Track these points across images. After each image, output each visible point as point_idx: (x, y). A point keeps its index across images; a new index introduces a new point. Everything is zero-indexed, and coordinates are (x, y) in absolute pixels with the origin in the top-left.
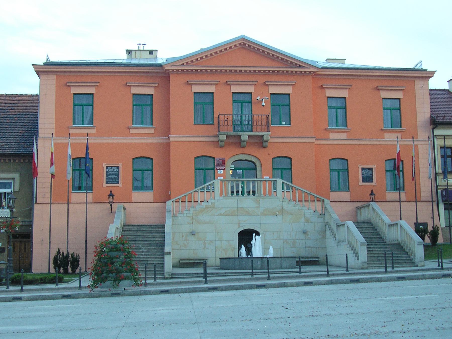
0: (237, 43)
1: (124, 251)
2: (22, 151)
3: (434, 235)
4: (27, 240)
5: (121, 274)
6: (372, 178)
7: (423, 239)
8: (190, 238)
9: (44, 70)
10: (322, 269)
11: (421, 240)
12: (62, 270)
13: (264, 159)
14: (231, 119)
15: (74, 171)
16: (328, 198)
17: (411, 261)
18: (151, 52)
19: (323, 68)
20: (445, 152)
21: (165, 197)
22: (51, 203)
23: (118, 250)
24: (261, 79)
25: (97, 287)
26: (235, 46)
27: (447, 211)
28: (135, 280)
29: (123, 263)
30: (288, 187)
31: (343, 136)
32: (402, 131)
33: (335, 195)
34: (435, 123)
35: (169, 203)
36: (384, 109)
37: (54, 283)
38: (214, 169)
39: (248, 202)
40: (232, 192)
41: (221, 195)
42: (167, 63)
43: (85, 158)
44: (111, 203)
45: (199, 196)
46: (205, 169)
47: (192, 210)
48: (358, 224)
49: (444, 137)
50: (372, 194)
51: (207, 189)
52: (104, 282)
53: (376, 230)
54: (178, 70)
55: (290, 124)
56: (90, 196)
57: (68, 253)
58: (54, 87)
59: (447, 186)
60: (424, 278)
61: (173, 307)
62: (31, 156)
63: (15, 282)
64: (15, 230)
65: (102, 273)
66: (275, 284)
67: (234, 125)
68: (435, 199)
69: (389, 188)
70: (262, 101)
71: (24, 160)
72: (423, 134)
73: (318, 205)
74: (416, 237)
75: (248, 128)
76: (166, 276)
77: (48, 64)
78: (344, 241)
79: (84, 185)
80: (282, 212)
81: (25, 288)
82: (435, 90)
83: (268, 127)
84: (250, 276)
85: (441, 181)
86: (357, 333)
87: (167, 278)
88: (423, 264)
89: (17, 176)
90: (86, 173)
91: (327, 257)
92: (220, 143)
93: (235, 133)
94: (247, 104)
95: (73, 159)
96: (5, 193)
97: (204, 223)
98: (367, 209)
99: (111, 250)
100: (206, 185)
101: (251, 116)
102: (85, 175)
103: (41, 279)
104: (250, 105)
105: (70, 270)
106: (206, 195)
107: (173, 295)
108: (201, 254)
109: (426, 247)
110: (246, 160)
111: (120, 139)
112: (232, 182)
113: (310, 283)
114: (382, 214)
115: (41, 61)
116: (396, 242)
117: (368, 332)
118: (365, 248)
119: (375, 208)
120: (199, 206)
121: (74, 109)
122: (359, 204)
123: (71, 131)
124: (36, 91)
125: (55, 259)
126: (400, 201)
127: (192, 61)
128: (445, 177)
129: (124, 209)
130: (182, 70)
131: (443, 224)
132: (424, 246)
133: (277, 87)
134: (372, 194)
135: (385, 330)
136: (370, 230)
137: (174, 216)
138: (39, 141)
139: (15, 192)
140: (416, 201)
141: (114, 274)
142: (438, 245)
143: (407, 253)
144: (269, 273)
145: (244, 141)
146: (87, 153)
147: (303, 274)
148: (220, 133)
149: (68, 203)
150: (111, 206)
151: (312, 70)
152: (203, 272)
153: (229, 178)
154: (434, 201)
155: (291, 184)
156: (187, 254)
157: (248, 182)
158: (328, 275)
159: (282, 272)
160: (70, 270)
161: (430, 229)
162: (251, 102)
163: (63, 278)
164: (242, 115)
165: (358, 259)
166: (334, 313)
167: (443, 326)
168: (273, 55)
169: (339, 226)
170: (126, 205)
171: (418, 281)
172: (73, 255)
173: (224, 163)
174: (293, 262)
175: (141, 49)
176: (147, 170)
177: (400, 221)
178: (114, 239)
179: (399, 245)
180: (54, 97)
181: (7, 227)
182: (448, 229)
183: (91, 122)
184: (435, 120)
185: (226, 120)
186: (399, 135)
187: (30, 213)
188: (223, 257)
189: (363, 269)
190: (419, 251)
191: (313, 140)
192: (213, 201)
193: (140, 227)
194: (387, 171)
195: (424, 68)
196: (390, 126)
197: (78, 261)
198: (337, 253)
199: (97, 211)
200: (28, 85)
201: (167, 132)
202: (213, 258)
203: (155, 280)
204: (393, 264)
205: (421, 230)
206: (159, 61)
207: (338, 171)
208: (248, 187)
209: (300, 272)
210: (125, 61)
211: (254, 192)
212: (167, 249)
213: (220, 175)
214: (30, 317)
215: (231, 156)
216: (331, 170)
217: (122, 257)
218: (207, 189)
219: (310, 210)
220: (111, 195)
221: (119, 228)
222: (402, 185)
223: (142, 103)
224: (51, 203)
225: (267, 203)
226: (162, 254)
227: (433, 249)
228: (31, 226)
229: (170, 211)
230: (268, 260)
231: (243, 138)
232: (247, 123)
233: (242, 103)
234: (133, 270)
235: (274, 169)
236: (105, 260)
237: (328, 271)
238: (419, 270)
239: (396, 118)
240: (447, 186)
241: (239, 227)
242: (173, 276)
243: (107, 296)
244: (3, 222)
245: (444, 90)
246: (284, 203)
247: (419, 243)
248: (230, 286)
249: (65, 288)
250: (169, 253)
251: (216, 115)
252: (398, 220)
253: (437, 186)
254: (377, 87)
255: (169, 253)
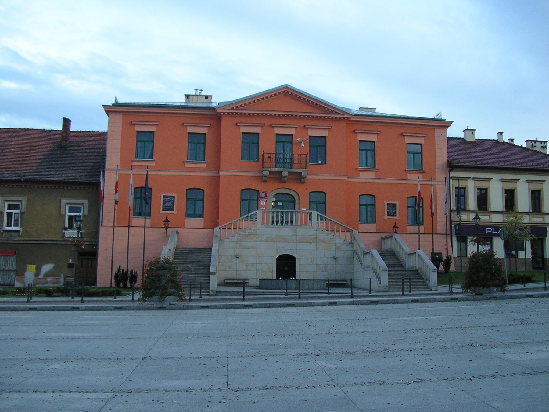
0: (281, 91)
1: (170, 270)
2: (92, 180)
3: (447, 263)
4: (93, 257)
5: (167, 290)
6: (396, 213)
7: (437, 266)
8: (235, 260)
9: (114, 110)
10: (348, 291)
11: (435, 267)
12: (121, 285)
13: (302, 193)
14: (274, 157)
15: (135, 198)
16: (357, 229)
17: (425, 286)
18: (207, 97)
19: (356, 115)
20: (459, 192)
21: (214, 224)
22: (114, 226)
23: (165, 269)
24: (301, 123)
25: (146, 301)
26: (280, 93)
27: (459, 243)
28: (180, 296)
29: (169, 281)
30: (322, 218)
31: (372, 175)
32: (422, 172)
33: (363, 227)
34: (451, 166)
35: (217, 229)
36: (408, 152)
37: (113, 296)
38: (258, 201)
39: (286, 231)
40: (273, 222)
41: (263, 223)
42: (220, 106)
43: (145, 187)
44: (167, 228)
45: (243, 224)
46: (249, 200)
47: (236, 236)
48: (382, 253)
49: (459, 179)
50: (395, 226)
51: (251, 217)
52: (152, 297)
53: (397, 258)
54: (228, 113)
55: (375, 167)
56: (148, 221)
57: (128, 270)
58: (120, 125)
59: (460, 221)
60: (435, 301)
61: (208, 322)
62: (99, 184)
63: (79, 293)
64: (81, 248)
65: (150, 289)
66: (303, 303)
67: (276, 163)
68: (449, 232)
69: (410, 223)
70: (301, 142)
71: (92, 188)
72: (441, 176)
73: (348, 235)
74: (432, 266)
75: (288, 165)
76: (211, 293)
77: (117, 105)
78: (369, 267)
79: (144, 211)
80: (316, 240)
81: (85, 299)
82: (452, 138)
83: (306, 165)
84: (284, 296)
85: (455, 217)
86: (369, 350)
87: (211, 295)
88: (436, 288)
89: (86, 202)
90: (145, 200)
91: (351, 281)
92: (264, 178)
93: (277, 170)
94: (288, 145)
95: (135, 188)
96: (76, 216)
97: (248, 247)
98: (390, 239)
99: (159, 269)
100: (250, 214)
101: (292, 155)
102: (144, 202)
103: (102, 292)
104: (291, 145)
105: (129, 285)
106: (250, 223)
107: (212, 310)
108: (243, 275)
109: (439, 274)
110: (286, 194)
111: (175, 172)
112: (273, 212)
113: (335, 304)
114: (404, 244)
115: (110, 102)
116: (414, 269)
117: (378, 350)
118: (386, 274)
119: (397, 239)
120: (243, 233)
121: (137, 144)
122: (384, 235)
123: (134, 164)
124: (105, 129)
125: (117, 275)
126: (419, 234)
127: (241, 106)
128: (459, 213)
129: (178, 233)
130: (232, 113)
131: (455, 255)
132: (438, 273)
133: (416, 138)
134: (395, 226)
135: (394, 347)
136: (393, 259)
137: (220, 240)
138: (106, 171)
139: (84, 216)
140: (433, 234)
141: (161, 290)
142: (450, 273)
143: (423, 279)
144: (299, 293)
145: (285, 177)
146: (147, 183)
147: (331, 295)
148: (265, 169)
149: (129, 227)
150: (166, 230)
151: (346, 116)
152: (242, 290)
153: (270, 209)
154: (448, 234)
155: (324, 216)
156: (231, 274)
157: (287, 213)
158: (352, 296)
159: (313, 293)
160: (129, 285)
161: (444, 258)
162: (291, 143)
163: (121, 292)
164: (283, 154)
165: (380, 283)
166: (352, 330)
167: (446, 345)
168: (313, 103)
169: (365, 254)
170: (179, 230)
171: (430, 303)
172: (132, 271)
173: (266, 196)
174: (324, 284)
175: (198, 94)
176: (199, 200)
177: (418, 251)
178: (161, 259)
179: (416, 272)
180: (120, 134)
181: (74, 245)
182: (459, 258)
183: (151, 156)
184: (451, 163)
185: (269, 158)
186: (420, 176)
187: (96, 235)
188: (262, 278)
189: (384, 291)
190: (433, 277)
191: (345, 178)
192: (255, 228)
193: (191, 250)
194: (408, 207)
195: (443, 118)
196: (412, 168)
197: (136, 278)
198: (362, 277)
199: (153, 234)
200: (100, 124)
201: (217, 167)
202: (254, 278)
203: (201, 297)
204: (410, 287)
205: (436, 259)
206: (213, 105)
207: (366, 205)
208: (287, 217)
209: (329, 293)
210: (183, 104)
211: (292, 222)
212: (212, 270)
213: (263, 206)
214: (81, 325)
215: (273, 189)
216: (360, 205)
217: (168, 275)
218: (251, 217)
219: (340, 239)
220: (167, 220)
221: (172, 250)
222: (421, 219)
223: (197, 140)
224: (114, 226)
225: (302, 232)
226: (208, 273)
227: (445, 277)
228: (96, 245)
229: (217, 236)
230: (299, 282)
231: (283, 174)
232: (288, 161)
233: (282, 142)
234: (178, 288)
235: (310, 202)
236: (153, 278)
237: (352, 293)
238: (432, 294)
239: (419, 162)
240: (460, 221)
241: (277, 252)
242: (217, 293)
243: (154, 309)
244: (71, 241)
245: (460, 138)
246: (318, 232)
247: (434, 271)
248: (263, 304)
249: (121, 301)
250: (214, 273)
251: (261, 153)
252: (417, 249)
253: (451, 221)
254: (354, 130)
255: (214, 273)
